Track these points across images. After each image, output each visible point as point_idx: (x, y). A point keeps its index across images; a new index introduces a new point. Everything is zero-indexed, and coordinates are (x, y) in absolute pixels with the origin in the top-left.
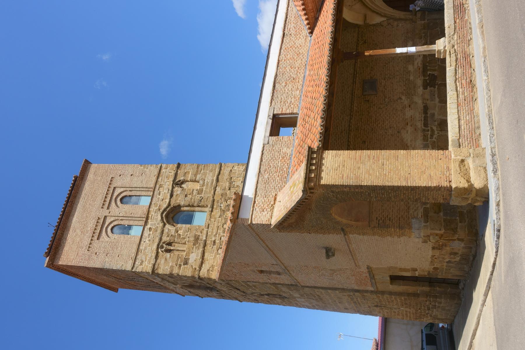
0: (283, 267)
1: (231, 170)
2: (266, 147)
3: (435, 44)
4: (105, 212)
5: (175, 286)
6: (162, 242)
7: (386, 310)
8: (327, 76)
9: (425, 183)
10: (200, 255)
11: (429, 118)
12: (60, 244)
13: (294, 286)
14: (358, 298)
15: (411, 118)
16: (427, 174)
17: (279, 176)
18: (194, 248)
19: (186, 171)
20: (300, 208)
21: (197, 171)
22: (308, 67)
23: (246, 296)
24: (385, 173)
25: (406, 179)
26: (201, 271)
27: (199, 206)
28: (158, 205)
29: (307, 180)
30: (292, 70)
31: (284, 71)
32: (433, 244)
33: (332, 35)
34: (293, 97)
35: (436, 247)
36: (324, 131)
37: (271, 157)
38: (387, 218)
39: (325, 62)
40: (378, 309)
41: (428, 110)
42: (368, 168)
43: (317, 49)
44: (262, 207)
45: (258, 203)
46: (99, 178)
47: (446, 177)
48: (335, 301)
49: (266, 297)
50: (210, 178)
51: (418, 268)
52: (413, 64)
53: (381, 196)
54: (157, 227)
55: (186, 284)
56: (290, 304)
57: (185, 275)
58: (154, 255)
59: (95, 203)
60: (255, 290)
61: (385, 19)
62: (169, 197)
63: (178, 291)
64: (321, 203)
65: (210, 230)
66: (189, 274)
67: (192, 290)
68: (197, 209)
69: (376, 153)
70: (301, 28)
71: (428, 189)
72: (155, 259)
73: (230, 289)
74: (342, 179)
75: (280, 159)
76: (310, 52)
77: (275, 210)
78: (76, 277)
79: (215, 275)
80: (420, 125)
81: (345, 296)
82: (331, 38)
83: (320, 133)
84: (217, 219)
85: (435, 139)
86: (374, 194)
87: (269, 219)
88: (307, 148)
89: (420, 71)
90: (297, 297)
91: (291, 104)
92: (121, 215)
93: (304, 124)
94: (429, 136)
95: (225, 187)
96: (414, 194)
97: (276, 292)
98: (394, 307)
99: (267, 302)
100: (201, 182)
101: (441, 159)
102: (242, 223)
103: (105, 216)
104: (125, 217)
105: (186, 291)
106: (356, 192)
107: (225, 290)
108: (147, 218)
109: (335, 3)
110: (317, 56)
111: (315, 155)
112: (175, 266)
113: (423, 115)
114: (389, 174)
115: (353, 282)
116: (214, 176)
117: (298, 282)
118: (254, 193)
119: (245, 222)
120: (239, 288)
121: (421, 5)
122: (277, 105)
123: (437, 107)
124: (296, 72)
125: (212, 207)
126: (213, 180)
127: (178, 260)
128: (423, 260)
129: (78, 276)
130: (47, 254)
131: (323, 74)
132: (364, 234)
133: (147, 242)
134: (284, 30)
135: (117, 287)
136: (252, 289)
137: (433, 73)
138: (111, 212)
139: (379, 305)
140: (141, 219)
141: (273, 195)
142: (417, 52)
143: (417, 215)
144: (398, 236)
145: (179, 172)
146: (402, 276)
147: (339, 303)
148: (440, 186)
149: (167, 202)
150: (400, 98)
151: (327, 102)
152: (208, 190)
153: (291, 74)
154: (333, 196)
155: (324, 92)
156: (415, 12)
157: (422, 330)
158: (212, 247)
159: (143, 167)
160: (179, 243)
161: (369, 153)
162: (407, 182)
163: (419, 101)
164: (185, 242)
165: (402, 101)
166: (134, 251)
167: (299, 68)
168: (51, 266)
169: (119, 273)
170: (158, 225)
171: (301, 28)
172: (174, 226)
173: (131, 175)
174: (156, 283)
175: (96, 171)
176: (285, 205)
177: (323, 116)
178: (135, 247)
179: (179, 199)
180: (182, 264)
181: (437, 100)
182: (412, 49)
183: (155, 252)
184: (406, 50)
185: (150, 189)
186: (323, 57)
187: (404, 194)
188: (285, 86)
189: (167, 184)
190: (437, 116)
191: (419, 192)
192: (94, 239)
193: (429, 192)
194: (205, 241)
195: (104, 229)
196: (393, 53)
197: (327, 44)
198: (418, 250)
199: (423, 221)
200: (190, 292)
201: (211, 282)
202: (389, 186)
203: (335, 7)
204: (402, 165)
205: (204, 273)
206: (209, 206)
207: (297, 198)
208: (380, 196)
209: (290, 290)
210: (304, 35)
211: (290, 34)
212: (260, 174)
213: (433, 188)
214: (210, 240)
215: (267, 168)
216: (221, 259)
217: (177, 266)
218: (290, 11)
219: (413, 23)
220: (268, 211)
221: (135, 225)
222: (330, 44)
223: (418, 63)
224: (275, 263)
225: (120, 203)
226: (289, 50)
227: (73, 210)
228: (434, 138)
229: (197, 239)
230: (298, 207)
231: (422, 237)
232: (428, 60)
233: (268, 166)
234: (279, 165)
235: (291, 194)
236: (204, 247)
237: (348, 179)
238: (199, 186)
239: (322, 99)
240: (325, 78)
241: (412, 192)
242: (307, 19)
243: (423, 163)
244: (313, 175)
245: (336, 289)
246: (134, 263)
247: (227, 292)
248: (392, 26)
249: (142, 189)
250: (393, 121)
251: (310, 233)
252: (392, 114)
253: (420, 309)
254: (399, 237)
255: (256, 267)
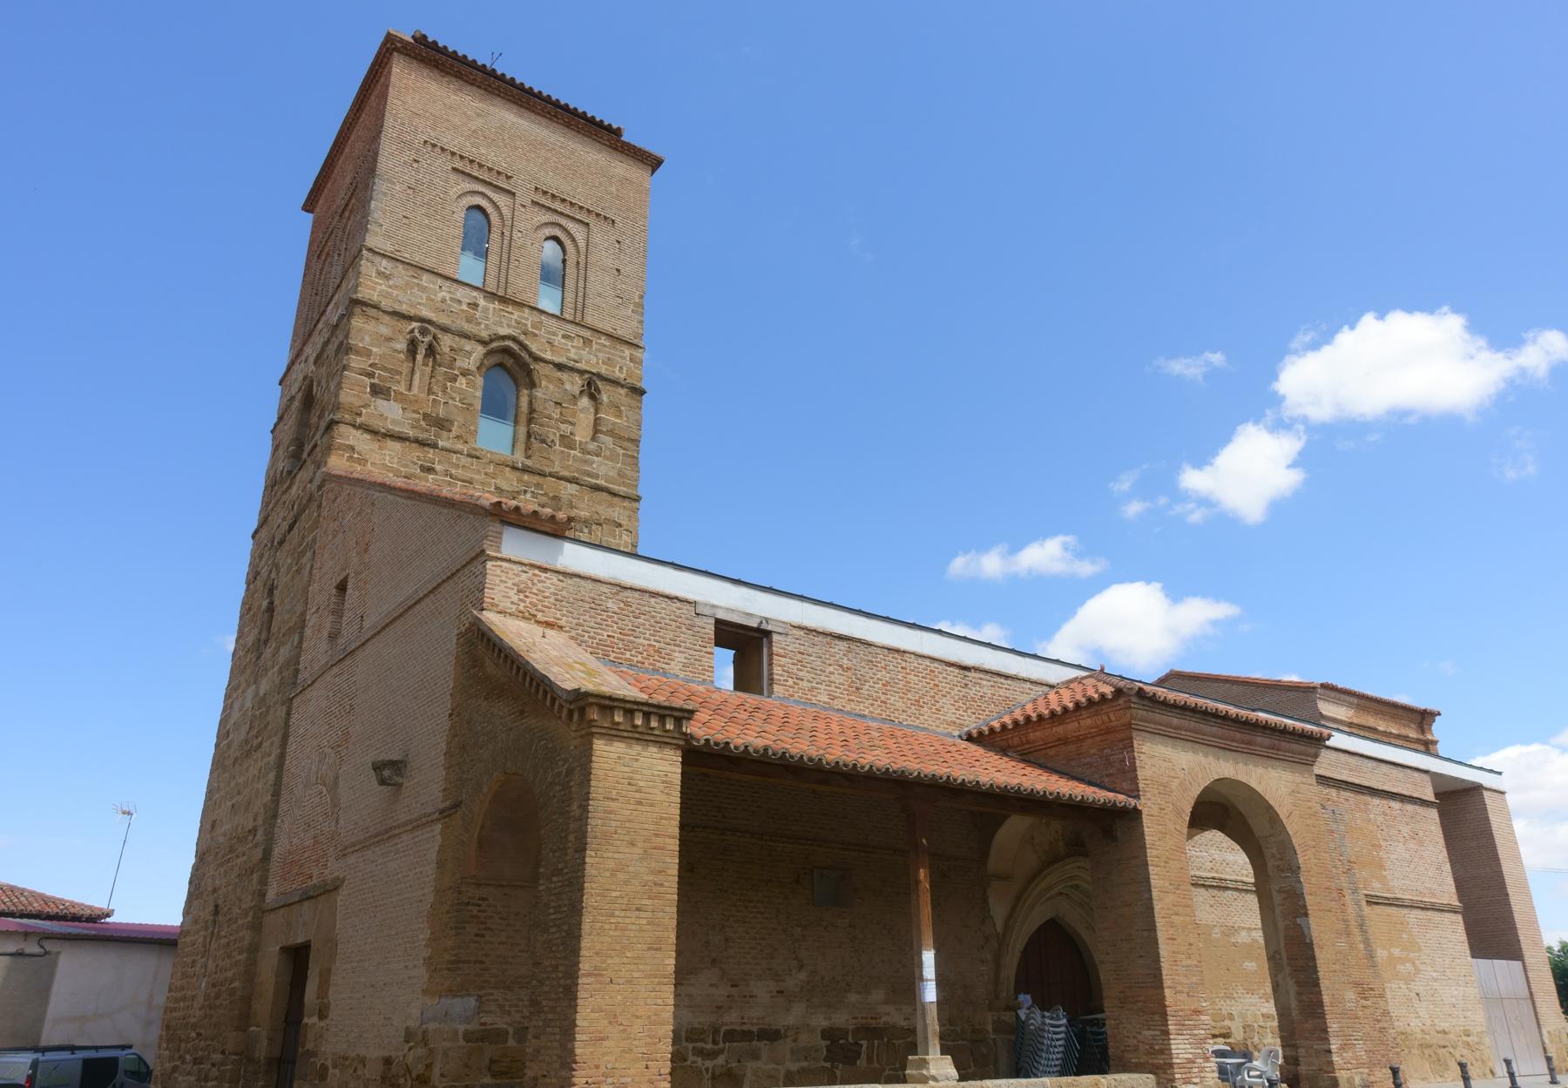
0: (353, 646)
1: (620, 525)
2: (687, 609)
3: (941, 1055)
4: (525, 196)
5: (312, 359)
6: (437, 332)
7: (201, 939)
8: (871, 766)
9: (585, 1024)
10: (397, 429)
11: (748, 1043)
12: (448, 73)
13: (292, 685)
14: (245, 858)
15: (751, 997)
16: (610, 1028)
17: (611, 639)
18: (416, 416)
19: (622, 408)
20: (527, 684)
21: (621, 438)
22: (887, 726)
23: (270, 549)
24: (617, 913)
25: (596, 973)
26: (351, 429)
27: (529, 435)
28: (537, 332)
29: (607, 702)
30: (880, 685)
31: (879, 665)
32: (401, 1059)
33: (970, 782)
34: (814, 685)
35: (390, 1069)
36: (732, 755)
37: (662, 621)
38: (483, 926)
39: (905, 764)
40: (206, 914)
41: (768, 1042)
42: (631, 869)
43: (933, 748)
44: (531, 588)
45: (543, 578)
46: (613, 190)
47: (598, 1083)
48: (239, 793)
49: (265, 604)
50: (602, 471)
51: (327, 1021)
52: (886, 1002)
53: (553, 904)
54: (479, 324)
55: (315, 387)
56: (237, 669)
57: (343, 385)
58: (404, 308)
59: (551, 173)
60: (288, 573)
61: (999, 929)
62: (557, 359)
63: (296, 367)
64: (540, 741)
65: (464, 460)
66: (348, 396)
67: (296, 404)
68: (522, 430)
69: (670, 890)
70: (981, 712)
71: (568, 1031)
72: (391, 310)
73: (293, 506)
74: (605, 798)
75: (655, 643)
76: (924, 733)
77: (523, 624)
78: (354, 105)
79: (337, 463)
80: (731, 1019)
81: (255, 820)
82: (964, 780)
83: (728, 743)
84: (493, 481)
85: (694, 1062)
86: (560, 884)
87: (498, 606)
88: (691, 708)
89: (869, 1020)
90: (258, 689)
91: (795, 680)
92: (516, 235)
93: (746, 708)
94: (700, 1045)
95: (577, 508)
96: (553, 996)
97: (276, 629)
98: (210, 962)
99: (247, 606)
100: (592, 446)
101: (647, 1068)
102: (490, 533)
103: (514, 194)
104: (510, 243)
105: (294, 389)
106: (566, 837)
107: (293, 494)
108: (504, 300)
109: (1048, 793)
110: (917, 748)
111: (672, 728)
112: (371, 362)
113: (755, 1029)
114: (613, 926)
115: (295, 840)
116: (606, 482)
117: (304, 690)
118: (568, 571)
119: (491, 541)
120: (295, 530)
121: (1032, 1021)
122: (794, 643)
123: (775, 1066)
124: (875, 694)
125: (525, 470)
126: (597, 476)
127: (385, 369)
128: (353, 1035)
129: (358, 111)
130: (421, 40)
131: (874, 758)
132: (441, 864)
133: (441, 295)
134: (977, 669)
135: (318, 209)
136: (290, 566)
137: (863, 1056)
138: (524, 210)
139: (220, 918)
140: (502, 284)
141: (561, 619)
142: (923, 1005)
143: (486, 1012)
144: (430, 958)
145: (623, 391)
146: (305, 978)
147: (233, 806)
148: (574, 1066)
149: (543, 356)
150: (801, 967)
151: (806, 764)
152: (570, 463)
153: (871, 684)
154: (559, 774)
155: (830, 758)
156: (1013, 1008)
157: (130, 1047)
158: (416, 464)
159: (637, 301)
160: (432, 377)
161: (670, 872)
162: (589, 975)
163: (791, 1017)
164: (433, 393)
165: (794, 971)
166: (418, 258)
167: (885, 703)
168: (389, 45)
169: (359, 217)
170: (483, 326)
171: (981, 712)
172: (478, 368)
173: (618, 270)
174: (324, 311)
175: (631, 183)
176: (534, 648)
177: (770, 753)
178: (429, 263)
179: (551, 387)
180: (376, 381)
181: (794, 1067)
182: (930, 994)
183: (413, 312)
184: (929, 977)
185: (579, 315)
186: (917, 761)
187: (556, 967)
188: (841, 666)
189: (592, 359)
190: (751, 1068)
191: (558, 1009)
192: (454, 159)
193: (558, 1037)
194: (434, 446)
195: (481, 188)
196: (924, 942)
197: (948, 770)
198: (385, 1018)
199: (469, 1027)
200: (292, 399)
201: (320, 455)
202: (580, 924)
203: (1038, 793)
204: (636, 962)
205: (348, 436)
206: (529, 463)
207: (556, 677)
208: (552, 901)
209: (280, 668)
210: (965, 720)
211: (966, 685)
212: (618, 588)
213: (569, 1045)
214: (437, 459)
215: (633, 609)
216: (386, 479)
217: (370, 366)
218: (1023, 688)
219: (987, 1002)
220: (519, 605)
221: (486, 269)
222: (948, 777)
223: (888, 1014)
224: (367, 624)
225: (548, 235)
226: (928, 681)
227: (533, 116)
228: (695, 1058)
229: (442, 424)
230: (532, 679)
231: (424, 1026)
232: (897, 1042)
233: (637, 611)
234: (641, 641)
235: (567, 664)
236: (417, 441)
237: (605, 812)
238: (584, 440)
239: (813, 752)
240: (866, 761)
241: (561, 990)
242: (1004, 726)
243: (638, 1017)
244: (618, 718)
245: (276, 794)
246: (384, 256)
247: (285, 497)
248: (983, 947)
249: (581, 294)
250: (744, 948)
251: (450, 715)
252: (760, 944)
253: (199, 1035)
254: (428, 961)
255: (358, 573)
